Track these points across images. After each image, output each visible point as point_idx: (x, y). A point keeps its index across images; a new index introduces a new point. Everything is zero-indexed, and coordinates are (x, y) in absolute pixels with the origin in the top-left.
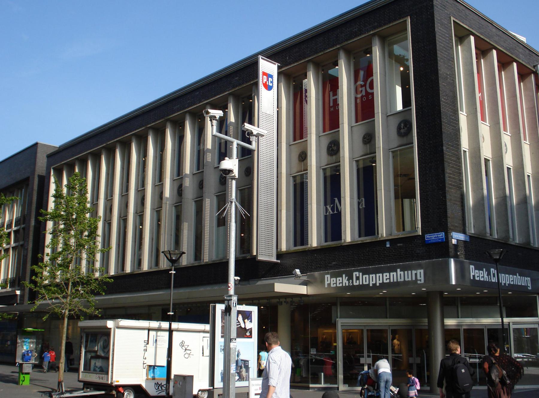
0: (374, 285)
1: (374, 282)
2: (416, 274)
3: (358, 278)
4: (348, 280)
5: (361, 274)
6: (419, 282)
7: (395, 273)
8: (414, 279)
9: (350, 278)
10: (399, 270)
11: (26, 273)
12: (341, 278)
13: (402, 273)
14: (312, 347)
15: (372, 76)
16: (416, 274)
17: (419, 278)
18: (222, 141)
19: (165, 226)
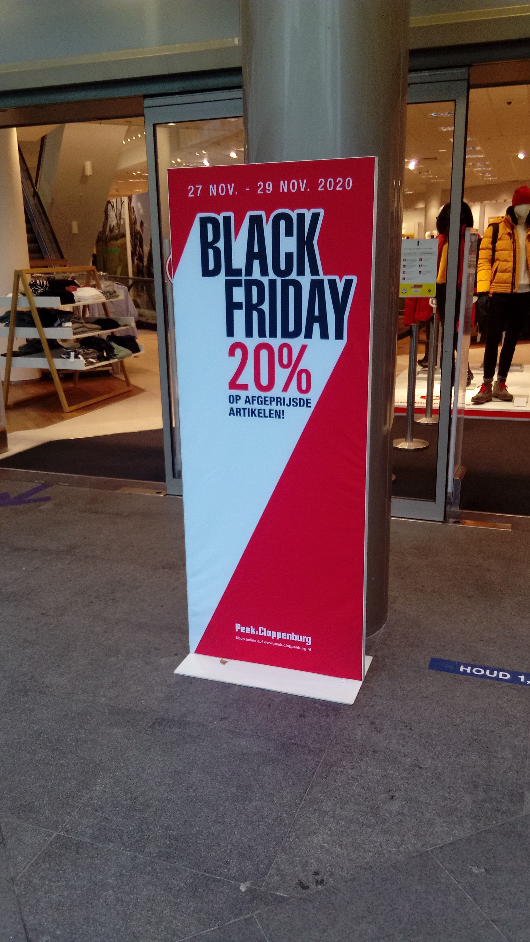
0: (275, 638)
1: (275, 636)
2: (305, 639)
3: (262, 631)
4: (255, 631)
5: (265, 629)
6: (307, 644)
7: (291, 635)
8: (304, 641)
9: (257, 629)
10: (293, 633)
11: (279, 359)
12: (249, 628)
13: (296, 636)
14: (367, 654)
15: (55, 340)
16: (305, 639)
17: (307, 641)
18: (52, 256)
19: (390, 421)
